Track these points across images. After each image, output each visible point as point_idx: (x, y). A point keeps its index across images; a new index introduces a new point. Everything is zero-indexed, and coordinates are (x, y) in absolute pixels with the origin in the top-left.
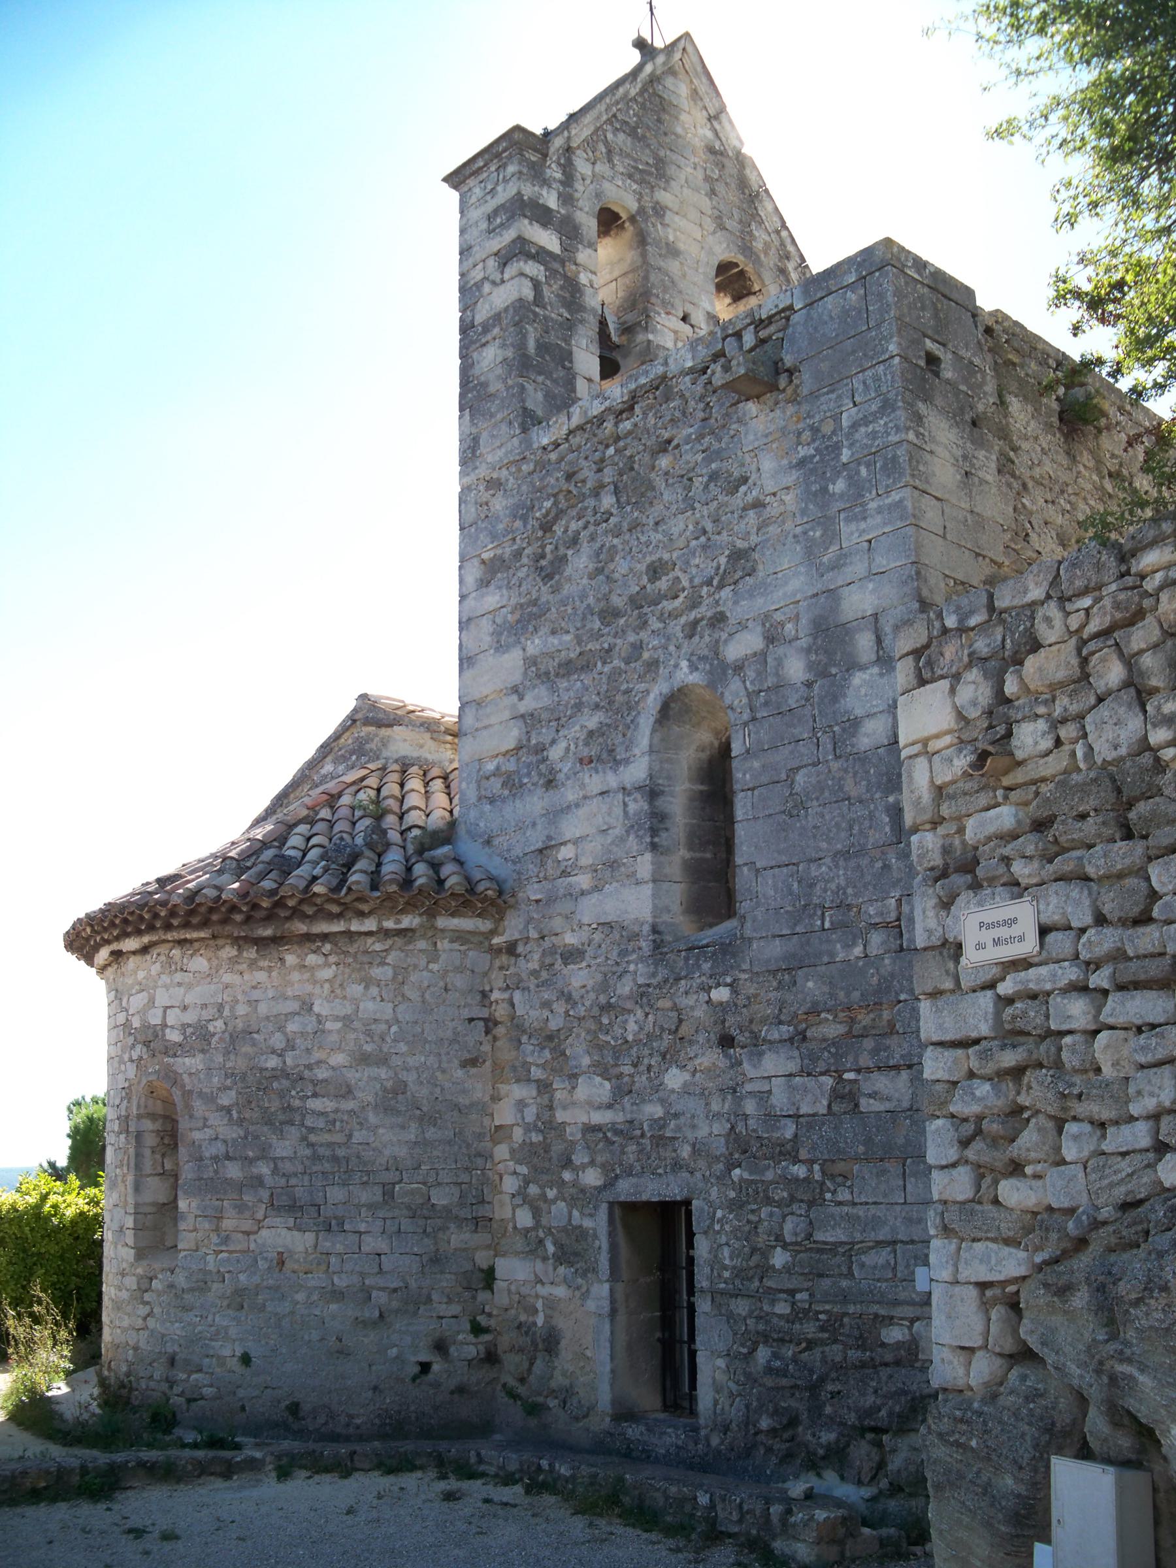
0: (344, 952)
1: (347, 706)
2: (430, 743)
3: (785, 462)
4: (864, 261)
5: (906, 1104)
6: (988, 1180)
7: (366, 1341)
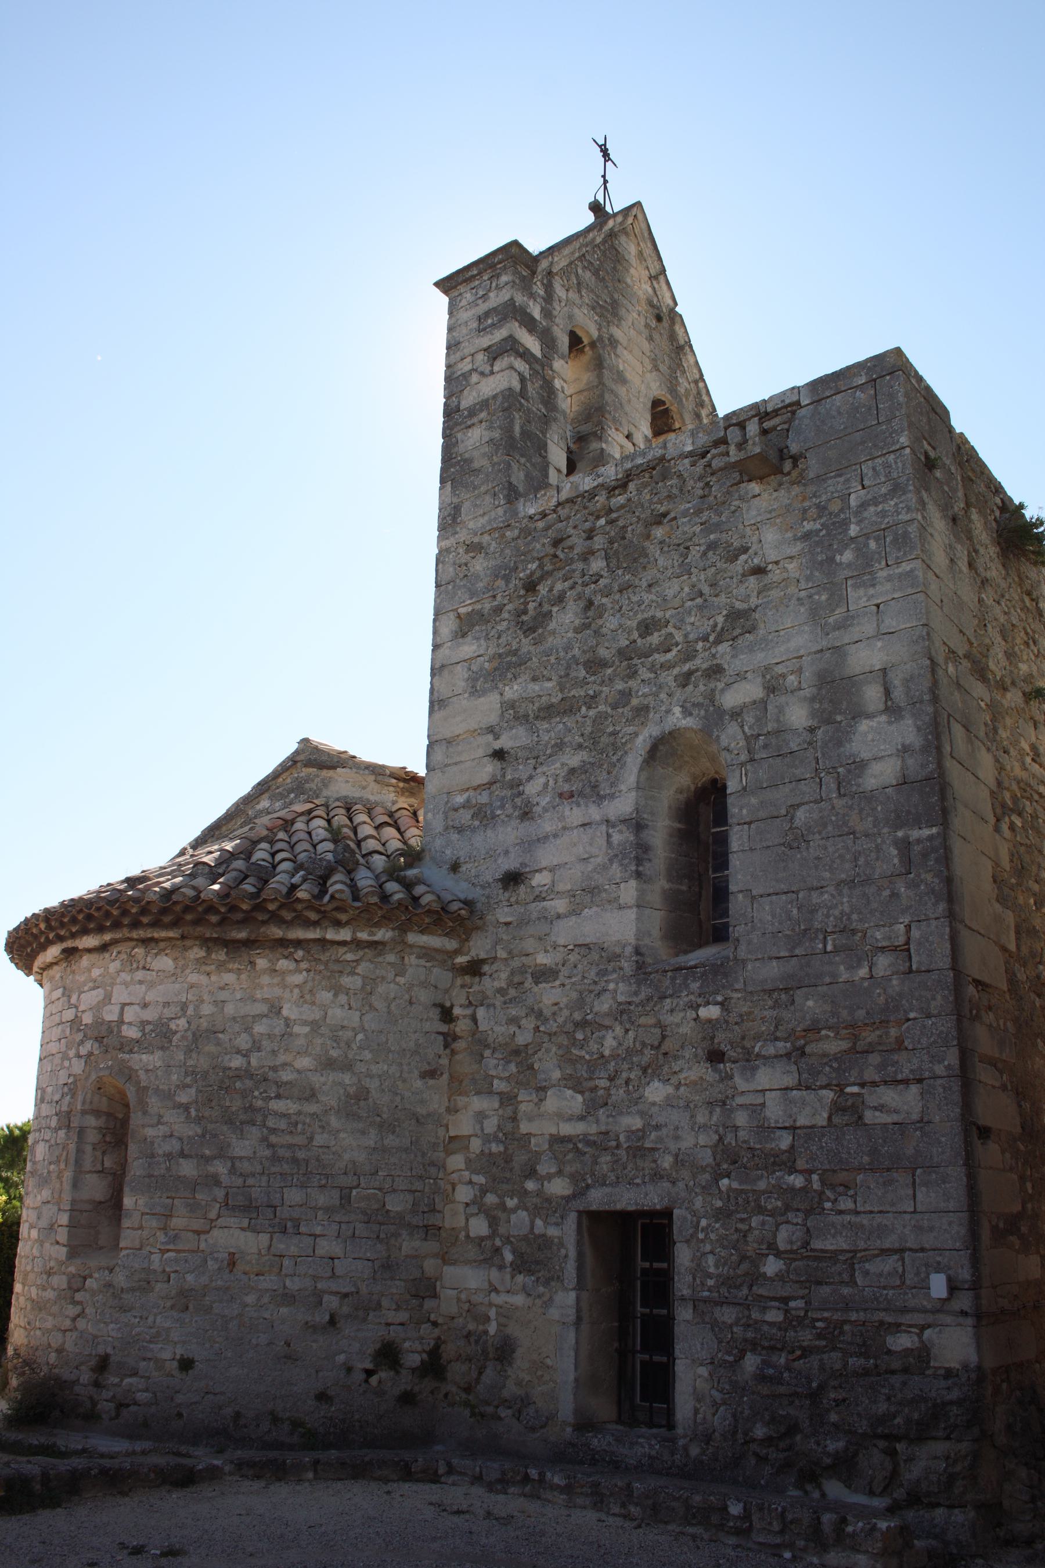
0: (315, 960)
1: (288, 748)
2: (373, 785)
3: (789, 535)
4: (875, 366)
5: (915, 1117)
7: (314, 1345)
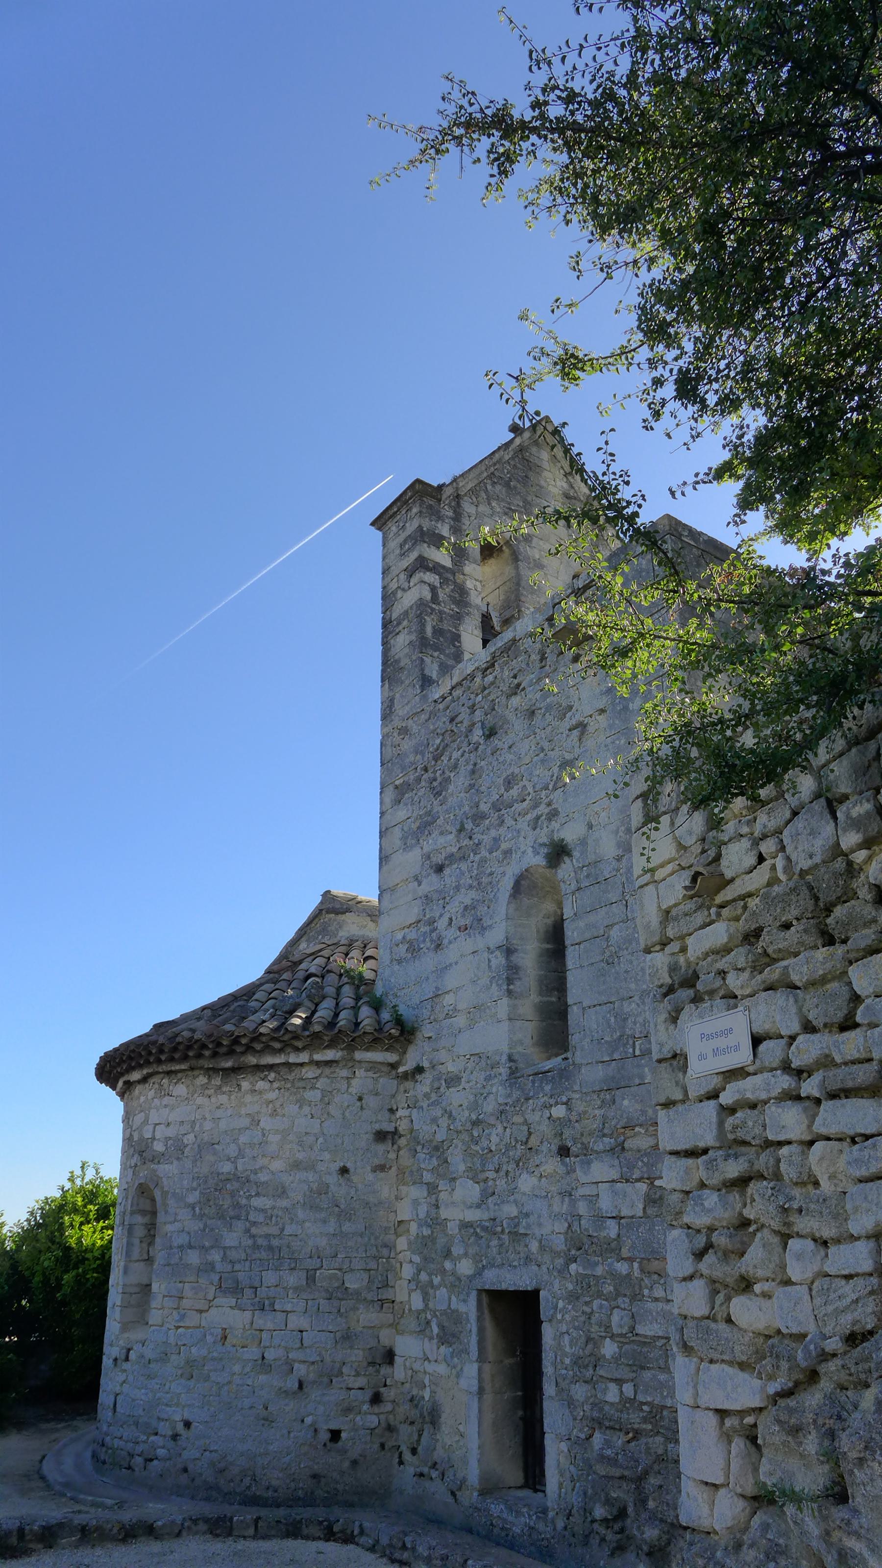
6: (720, 1298)
